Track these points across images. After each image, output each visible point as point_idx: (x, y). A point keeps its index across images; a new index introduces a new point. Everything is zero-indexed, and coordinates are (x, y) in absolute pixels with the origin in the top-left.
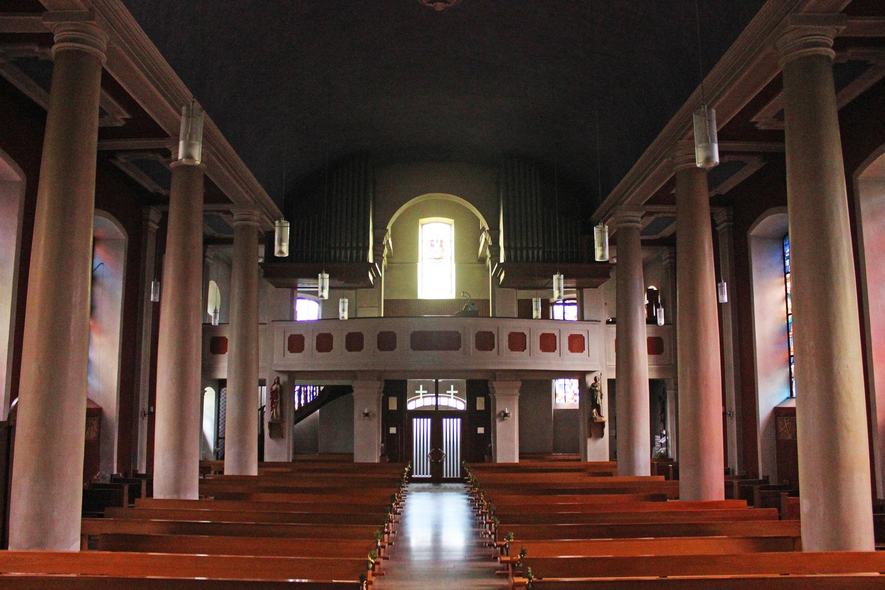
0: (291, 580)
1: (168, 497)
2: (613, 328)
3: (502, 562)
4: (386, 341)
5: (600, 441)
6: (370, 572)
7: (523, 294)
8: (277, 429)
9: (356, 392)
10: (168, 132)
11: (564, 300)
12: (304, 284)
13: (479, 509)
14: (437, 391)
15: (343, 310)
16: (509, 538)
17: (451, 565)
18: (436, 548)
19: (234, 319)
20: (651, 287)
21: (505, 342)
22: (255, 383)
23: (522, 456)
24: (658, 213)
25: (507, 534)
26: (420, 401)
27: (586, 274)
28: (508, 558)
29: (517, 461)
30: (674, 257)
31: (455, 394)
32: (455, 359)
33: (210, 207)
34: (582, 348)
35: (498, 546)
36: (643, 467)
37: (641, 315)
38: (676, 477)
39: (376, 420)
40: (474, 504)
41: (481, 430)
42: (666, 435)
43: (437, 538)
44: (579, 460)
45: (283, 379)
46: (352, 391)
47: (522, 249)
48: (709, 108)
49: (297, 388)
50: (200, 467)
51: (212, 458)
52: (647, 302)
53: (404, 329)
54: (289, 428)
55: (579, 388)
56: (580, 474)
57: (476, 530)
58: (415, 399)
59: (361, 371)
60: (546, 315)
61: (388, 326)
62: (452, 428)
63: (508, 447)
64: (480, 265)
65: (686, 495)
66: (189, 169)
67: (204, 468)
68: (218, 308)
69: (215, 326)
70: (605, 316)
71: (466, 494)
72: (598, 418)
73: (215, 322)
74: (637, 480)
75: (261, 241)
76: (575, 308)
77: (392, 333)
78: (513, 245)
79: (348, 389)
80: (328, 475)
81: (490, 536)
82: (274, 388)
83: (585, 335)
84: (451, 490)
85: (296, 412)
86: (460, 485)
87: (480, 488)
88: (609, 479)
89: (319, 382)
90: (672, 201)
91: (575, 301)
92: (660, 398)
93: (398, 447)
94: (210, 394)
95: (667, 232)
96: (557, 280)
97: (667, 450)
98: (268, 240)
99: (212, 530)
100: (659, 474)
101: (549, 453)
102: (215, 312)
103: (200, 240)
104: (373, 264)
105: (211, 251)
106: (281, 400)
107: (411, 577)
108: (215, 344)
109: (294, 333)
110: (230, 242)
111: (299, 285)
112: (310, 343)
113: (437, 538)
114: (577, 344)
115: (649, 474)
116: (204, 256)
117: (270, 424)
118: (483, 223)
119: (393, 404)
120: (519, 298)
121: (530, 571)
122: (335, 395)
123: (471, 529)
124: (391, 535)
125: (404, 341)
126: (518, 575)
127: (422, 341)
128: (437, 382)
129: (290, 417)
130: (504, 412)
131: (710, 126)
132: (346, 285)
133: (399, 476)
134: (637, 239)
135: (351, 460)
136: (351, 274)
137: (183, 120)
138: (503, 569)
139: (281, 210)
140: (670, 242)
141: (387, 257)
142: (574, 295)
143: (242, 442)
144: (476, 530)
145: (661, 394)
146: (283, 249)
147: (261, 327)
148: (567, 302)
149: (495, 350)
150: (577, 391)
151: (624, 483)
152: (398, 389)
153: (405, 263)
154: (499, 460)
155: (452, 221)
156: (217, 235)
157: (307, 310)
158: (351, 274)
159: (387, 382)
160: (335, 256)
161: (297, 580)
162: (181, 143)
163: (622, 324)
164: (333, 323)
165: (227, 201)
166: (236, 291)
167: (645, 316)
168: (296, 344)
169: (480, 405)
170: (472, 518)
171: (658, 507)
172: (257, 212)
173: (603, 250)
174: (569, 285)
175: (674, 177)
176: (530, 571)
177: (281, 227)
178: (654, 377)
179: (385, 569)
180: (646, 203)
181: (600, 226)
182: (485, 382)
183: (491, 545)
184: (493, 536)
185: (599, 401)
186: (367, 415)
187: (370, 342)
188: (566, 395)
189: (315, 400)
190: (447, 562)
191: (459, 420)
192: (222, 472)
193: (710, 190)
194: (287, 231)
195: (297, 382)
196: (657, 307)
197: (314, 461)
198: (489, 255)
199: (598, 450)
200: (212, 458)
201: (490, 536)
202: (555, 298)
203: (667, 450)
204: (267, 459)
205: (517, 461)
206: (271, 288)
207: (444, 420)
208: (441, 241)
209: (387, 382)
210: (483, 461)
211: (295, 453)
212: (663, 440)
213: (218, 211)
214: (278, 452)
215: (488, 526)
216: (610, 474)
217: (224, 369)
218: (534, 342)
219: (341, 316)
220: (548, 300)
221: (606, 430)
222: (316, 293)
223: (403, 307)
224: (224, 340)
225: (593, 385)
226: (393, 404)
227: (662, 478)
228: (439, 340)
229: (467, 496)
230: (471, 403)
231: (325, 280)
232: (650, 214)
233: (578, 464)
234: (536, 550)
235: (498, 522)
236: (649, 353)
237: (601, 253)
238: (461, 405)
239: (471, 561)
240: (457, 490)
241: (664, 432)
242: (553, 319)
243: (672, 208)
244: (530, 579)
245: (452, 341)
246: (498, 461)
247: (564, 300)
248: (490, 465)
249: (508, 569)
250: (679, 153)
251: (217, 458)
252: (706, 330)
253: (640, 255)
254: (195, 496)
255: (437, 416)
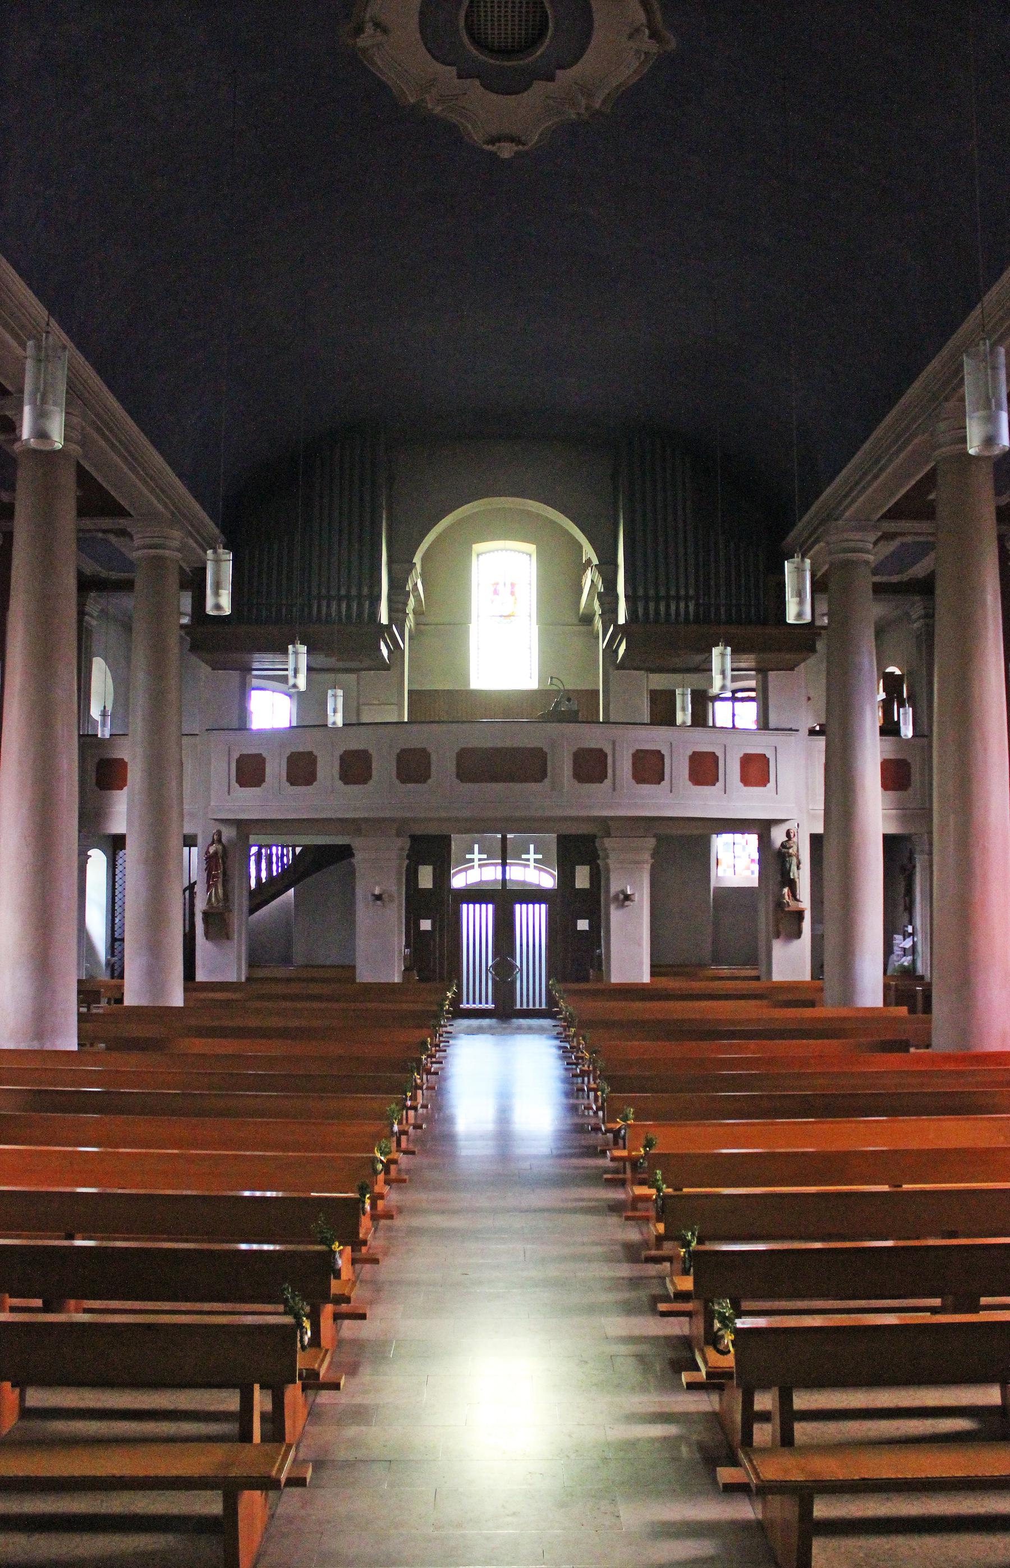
0: (247, 1193)
1: (23, 1046)
2: (821, 742)
3: (613, 1159)
4: (413, 766)
5: (796, 943)
6: (381, 1177)
7: (659, 681)
8: (217, 923)
9: (359, 858)
10: (10, 389)
11: (734, 692)
12: (263, 661)
13: (577, 1064)
14: (504, 855)
15: (335, 711)
16: (625, 1119)
17: (526, 1165)
18: (504, 1135)
19: (138, 725)
20: (890, 669)
21: (625, 767)
22: (176, 841)
23: (656, 970)
24: (902, 534)
25: (622, 1111)
26: (473, 872)
27: (772, 646)
28: (624, 1153)
29: (646, 979)
30: (929, 615)
31: (536, 861)
32: (533, 798)
33: (88, 523)
34: (765, 775)
35: (608, 1131)
36: (870, 989)
37: (871, 719)
38: (928, 1009)
39: (395, 905)
40: (569, 1055)
41: (583, 925)
42: (912, 934)
43: (504, 1116)
44: (758, 978)
45: (229, 833)
46: (352, 855)
47: (657, 600)
48: (994, 346)
49: (254, 850)
50: (79, 992)
51: (103, 975)
52: (882, 695)
53: (443, 746)
54: (239, 920)
55: (759, 850)
56: (758, 1002)
57: (572, 1101)
58: (466, 870)
59: (366, 820)
60: (700, 718)
61: (418, 738)
62: (531, 921)
63: (630, 953)
64: (583, 628)
65: (942, 1041)
66: (47, 458)
67: (87, 993)
68: (109, 708)
69: (103, 740)
70: (810, 720)
71: (557, 1038)
72: (792, 903)
73: (104, 732)
74: (861, 1014)
75: (183, 586)
76: (753, 706)
77: (424, 750)
78: (641, 592)
79: (345, 852)
80: (315, 1005)
81: (596, 1113)
82: (212, 850)
83: (770, 754)
84: (530, 1030)
85: (252, 894)
86: (546, 1023)
87: (579, 1028)
88: (807, 1013)
89: (289, 839)
90: (928, 513)
91: (753, 694)
92: (903, 869)
93: (434, 957)
94: (97, 861)
95: (919, 570)
96: (720, 657)
97: (914, 961)
98: (195, 582)
99: (107, 1104)
100: (898, 1004)
101: (701, 966)
102: (104, 714)
103: (70, 583)
104: (388, 627)
105: (94, 605)
106: (225, 874)
107: (455, 1185)
108: (103, 773)
109: (246, 752)
110: (126, 586)
111: (256, 665)
112: (275, 769)
113: (504, 1116)
114: (756, 770)
115: (880, 1004)
116: (81, 613)
117: (206, 915)
118: (589, 552)
119: (426, 879)
120: (652, 687)
121: (659, 1177)
122: (321, 863)
123: (564, 1101)
124: (420, 1111)
125: (443, 767)
126: (642, 1183)
127: (482, 766)
128: (504, 839)
129: (240, 902)
130: (623, 892)
131: (995, 378)
132: (340, 665)
133: (435, 1008)
134: (865, 581)
135: (352, 979)
136: (349, 644)
137: (29, 365)
138: (616, 1171)
139: (217, 524)
140: (925, 588)
141: (415, 612)
142: (752, 684)
143: (155, 948)
144: (572, 1101)
145: (905, 861)
146: (221, 601)
147: (185, 740)
148: (739, 695)
149: (608, 782)
150: (756, 856)
151: (831, 1019)
152: (433, 850)
153: (445, 626)
154: (615, 978)
155: (532, 548)
156: (104, 574)
157: (270, 710)
158: (349, 644)
159: (415, 839)
160: (319, 611)
161: (258, 1194)
162: (27, 410)
163: (837, 735)
164: (318, 733)
165: (121, 512)
166: (141, 678)
167: (879, 723)
168: (250, 771)
169: (582, 879)
170: (566, 1081)
171: (893, 1061)
172: (177, 534)
173: (801, 603)
174: (743, 665)
175: (934, 470)
176: (659, 1177)
177: (217, 561)
178: (892, 830)
179: (408, 1171)
180: (884, 517)
181: (797, 559)
182: (591, 839)
183: (596, 1129)
184: (600, 1113)
185: (794, 873)
186: (378, 898)
187: (384, 768)
188: (735, 862)
189: (285, 871)
190: (526, 1158)
191: (543, 906)
192: (120, 1000)
193: (998, 493)
194: (228, 569)
195: (252, 839)
196: (901, 705)
197: (289, 980)
198: (598, 611)
199: (791, 961)
200: (103, 975)
201: (596, 1113)
202: (715, 690)
203: (914, 961)
204: (200, 976)
205: (646, 979)
206: (205, 669)
207: (517, 907)
208: (513, 585)
209: (415, 839)
210: (586, 979)
211: (251, 965)
212: (908, 943)
213: (105, 531)
214: (220, 964)
215: (592, 1094)
216: (812, 1004)
217: (122, 814)
218: (678, 767)
219: (330, 720)
220: (705, 692)
221: (807, 925)
222: (284, 679)
223: (443, 705)
224: (122, 764)
225: (783, 845)
226: (426, 879)
227: (903, 1011)
228: (505, 762)
229: (557, 1042)
230: (566, 877)
231: (299, 656)
232: (887, 537)
233: (754, 984)
234: (672, 1139)
235: (608, 1090)
236: (885, 786)
237: (796, 610)
238: (547, 881)
239: (565, 1156)
240: (541, 1031)
241: (910, 929)
242: (714, 726)
243: (925, 526)
244: (659, 1190)
245: (526, 765)
246: (614, 980)
247: (734, 692)
248: (599, 986)
249: (625, 1172)
250: (942, 426)
251: (113, 977)
252: (985, 749)
253: (872, 611)
254: (71, 1044)
255: (504, 899)
